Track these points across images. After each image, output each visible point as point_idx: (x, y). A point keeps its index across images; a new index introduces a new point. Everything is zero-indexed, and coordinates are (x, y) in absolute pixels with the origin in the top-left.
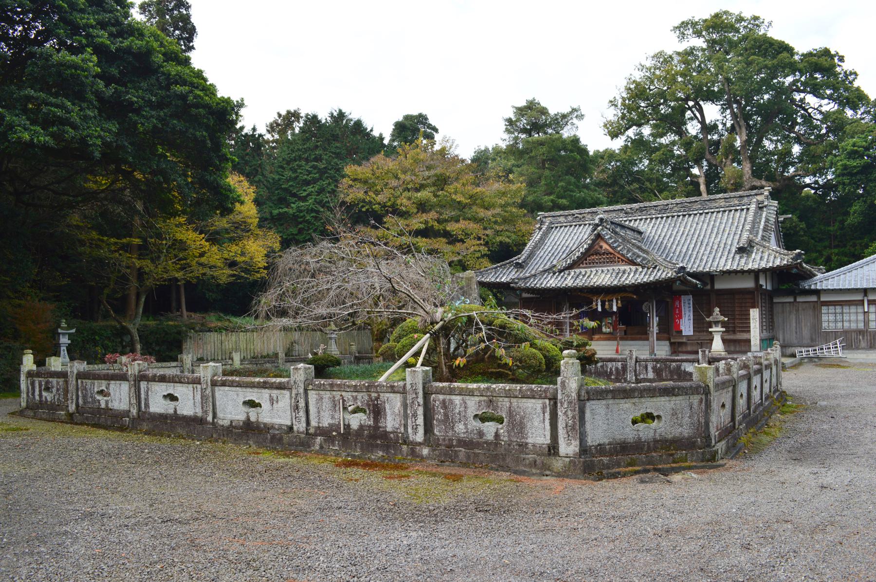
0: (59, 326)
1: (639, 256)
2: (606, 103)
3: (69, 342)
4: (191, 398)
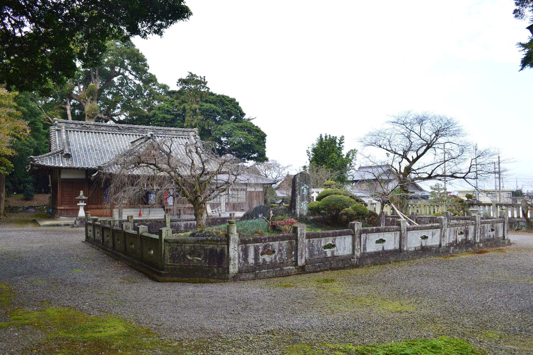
4: (393, 239)
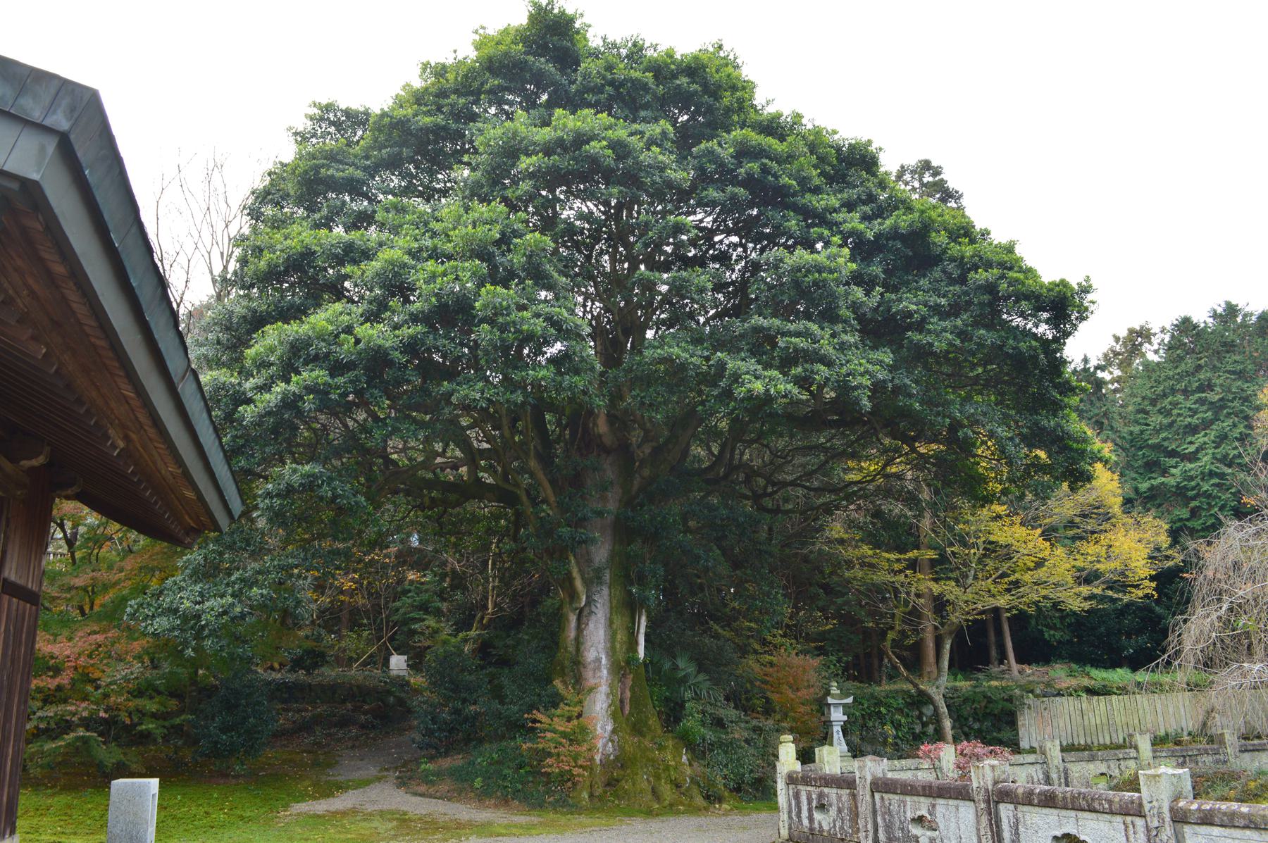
0: (828, 693)
3: (845, 718)
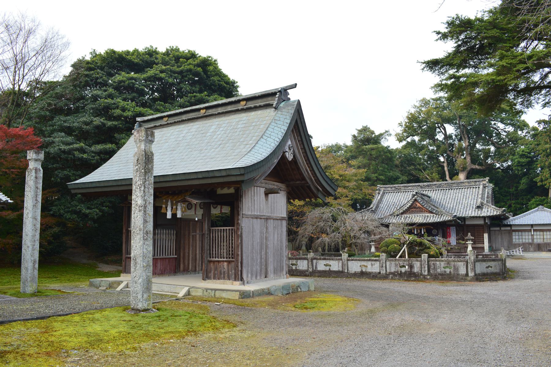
1: (434, 210)
2: (397, 125)
